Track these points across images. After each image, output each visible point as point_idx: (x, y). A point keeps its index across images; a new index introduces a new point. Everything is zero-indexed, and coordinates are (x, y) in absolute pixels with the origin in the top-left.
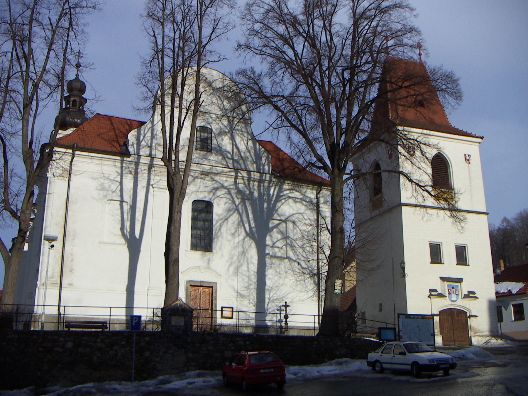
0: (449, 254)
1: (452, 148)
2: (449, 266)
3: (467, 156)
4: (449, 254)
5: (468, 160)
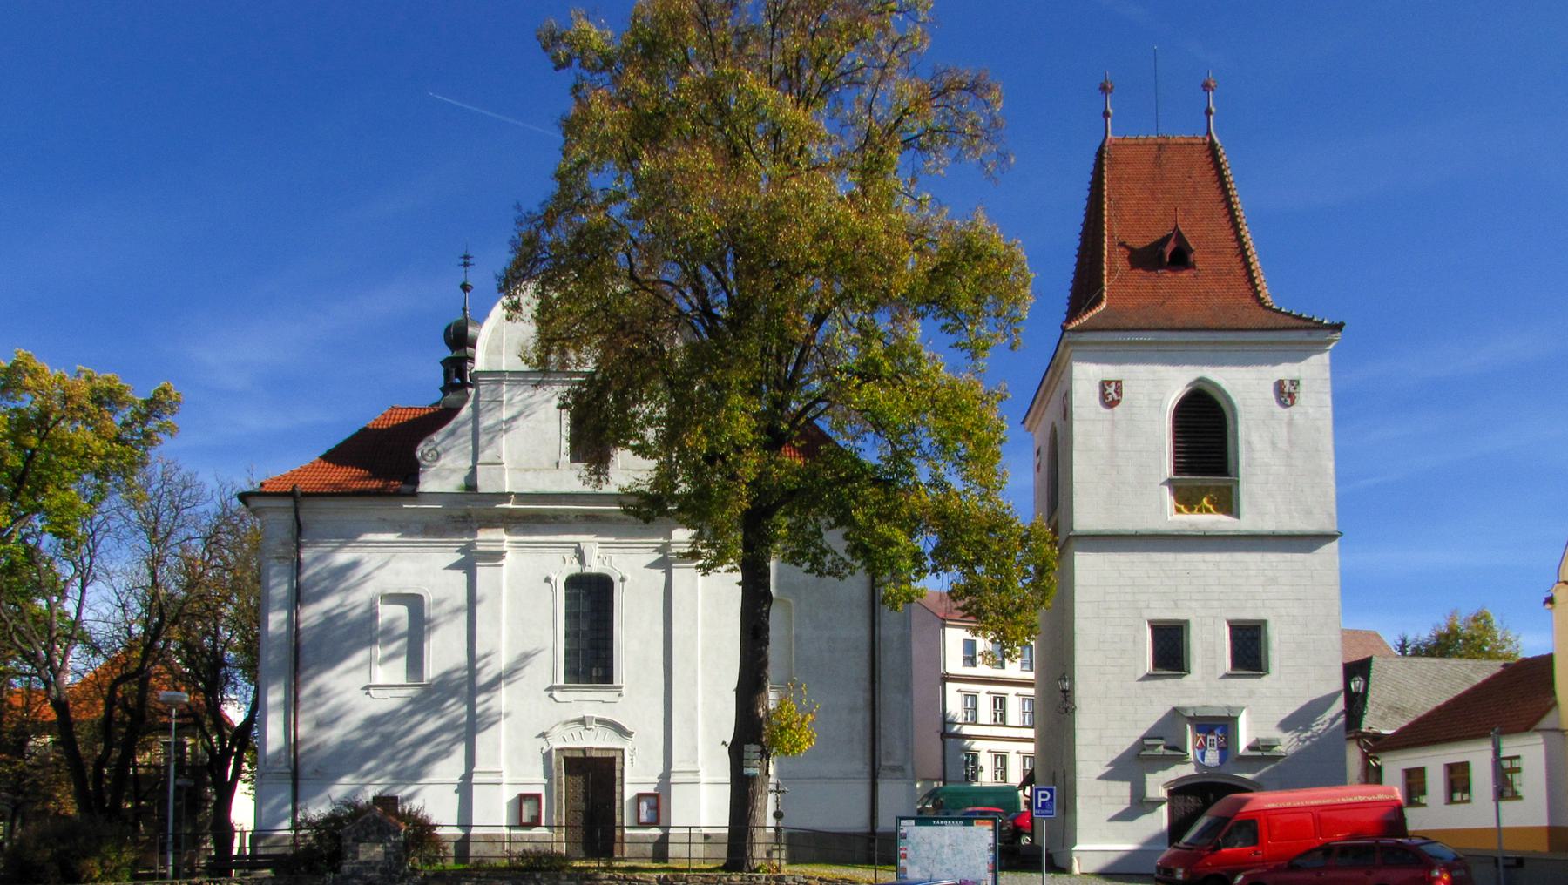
0: (1210, 647)
1: (1244, 385)
2: (1207, 681)
3: (1287, 384)
4: (1210, 647)
5: (1291, 395)
